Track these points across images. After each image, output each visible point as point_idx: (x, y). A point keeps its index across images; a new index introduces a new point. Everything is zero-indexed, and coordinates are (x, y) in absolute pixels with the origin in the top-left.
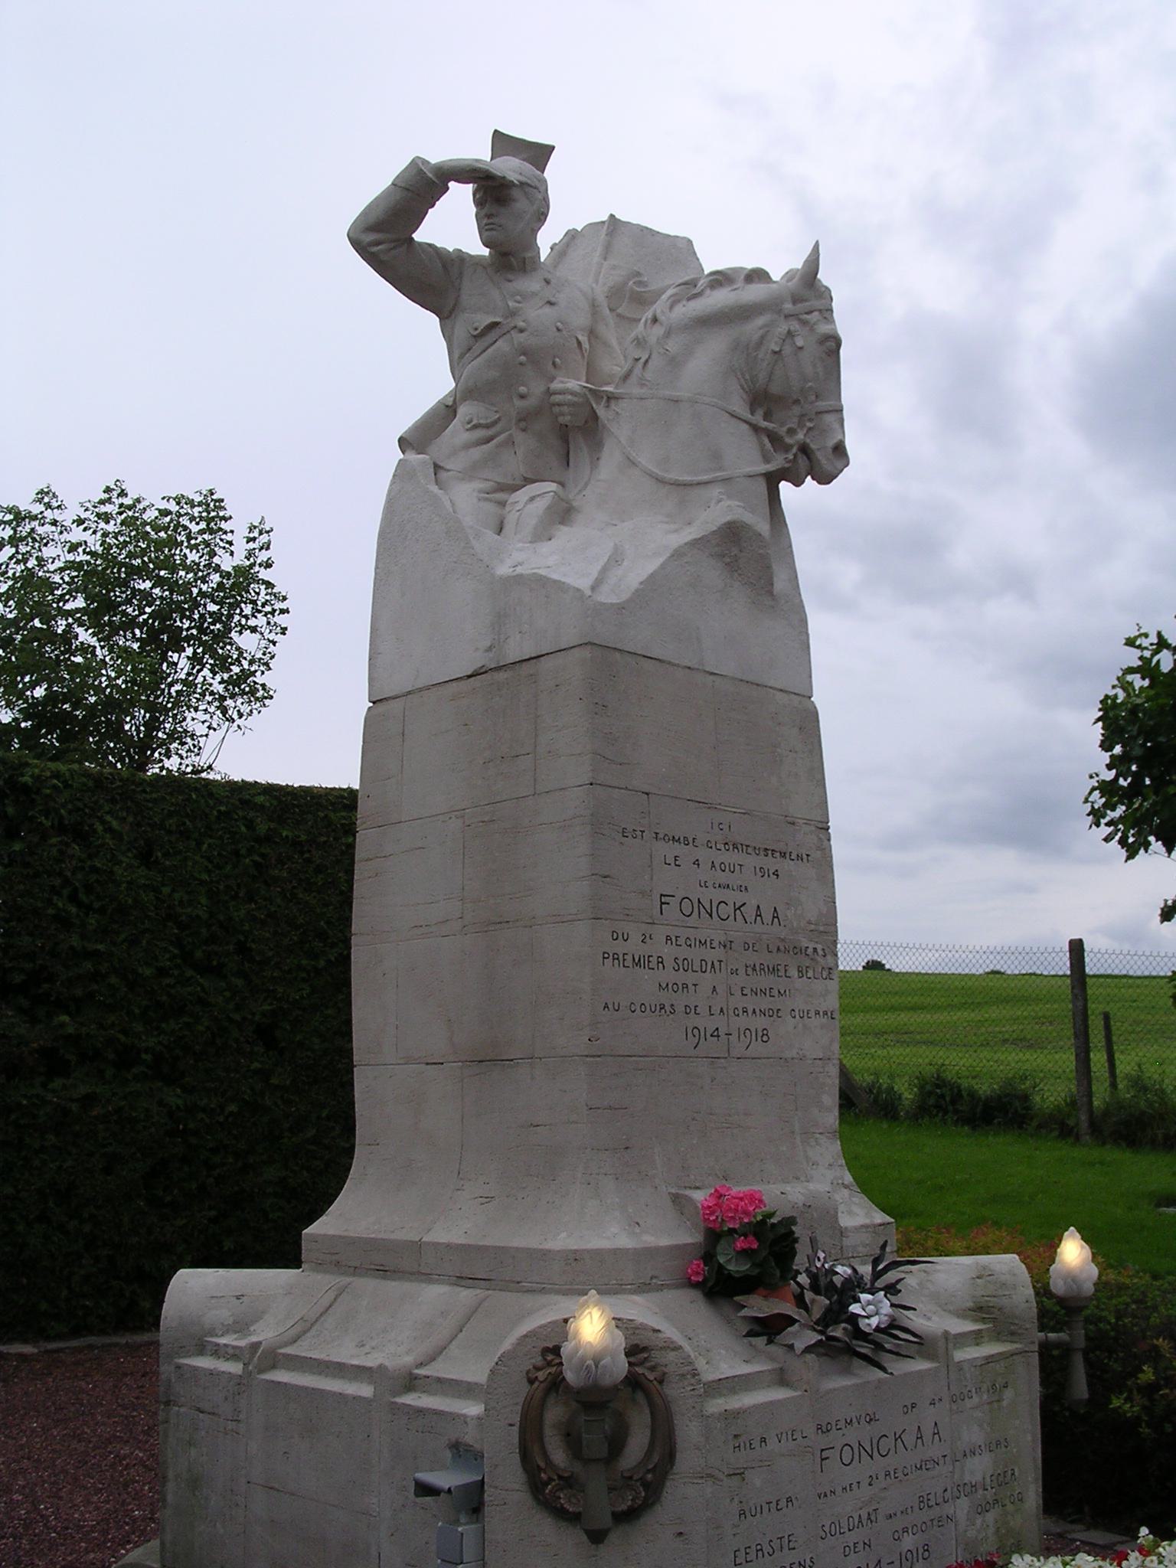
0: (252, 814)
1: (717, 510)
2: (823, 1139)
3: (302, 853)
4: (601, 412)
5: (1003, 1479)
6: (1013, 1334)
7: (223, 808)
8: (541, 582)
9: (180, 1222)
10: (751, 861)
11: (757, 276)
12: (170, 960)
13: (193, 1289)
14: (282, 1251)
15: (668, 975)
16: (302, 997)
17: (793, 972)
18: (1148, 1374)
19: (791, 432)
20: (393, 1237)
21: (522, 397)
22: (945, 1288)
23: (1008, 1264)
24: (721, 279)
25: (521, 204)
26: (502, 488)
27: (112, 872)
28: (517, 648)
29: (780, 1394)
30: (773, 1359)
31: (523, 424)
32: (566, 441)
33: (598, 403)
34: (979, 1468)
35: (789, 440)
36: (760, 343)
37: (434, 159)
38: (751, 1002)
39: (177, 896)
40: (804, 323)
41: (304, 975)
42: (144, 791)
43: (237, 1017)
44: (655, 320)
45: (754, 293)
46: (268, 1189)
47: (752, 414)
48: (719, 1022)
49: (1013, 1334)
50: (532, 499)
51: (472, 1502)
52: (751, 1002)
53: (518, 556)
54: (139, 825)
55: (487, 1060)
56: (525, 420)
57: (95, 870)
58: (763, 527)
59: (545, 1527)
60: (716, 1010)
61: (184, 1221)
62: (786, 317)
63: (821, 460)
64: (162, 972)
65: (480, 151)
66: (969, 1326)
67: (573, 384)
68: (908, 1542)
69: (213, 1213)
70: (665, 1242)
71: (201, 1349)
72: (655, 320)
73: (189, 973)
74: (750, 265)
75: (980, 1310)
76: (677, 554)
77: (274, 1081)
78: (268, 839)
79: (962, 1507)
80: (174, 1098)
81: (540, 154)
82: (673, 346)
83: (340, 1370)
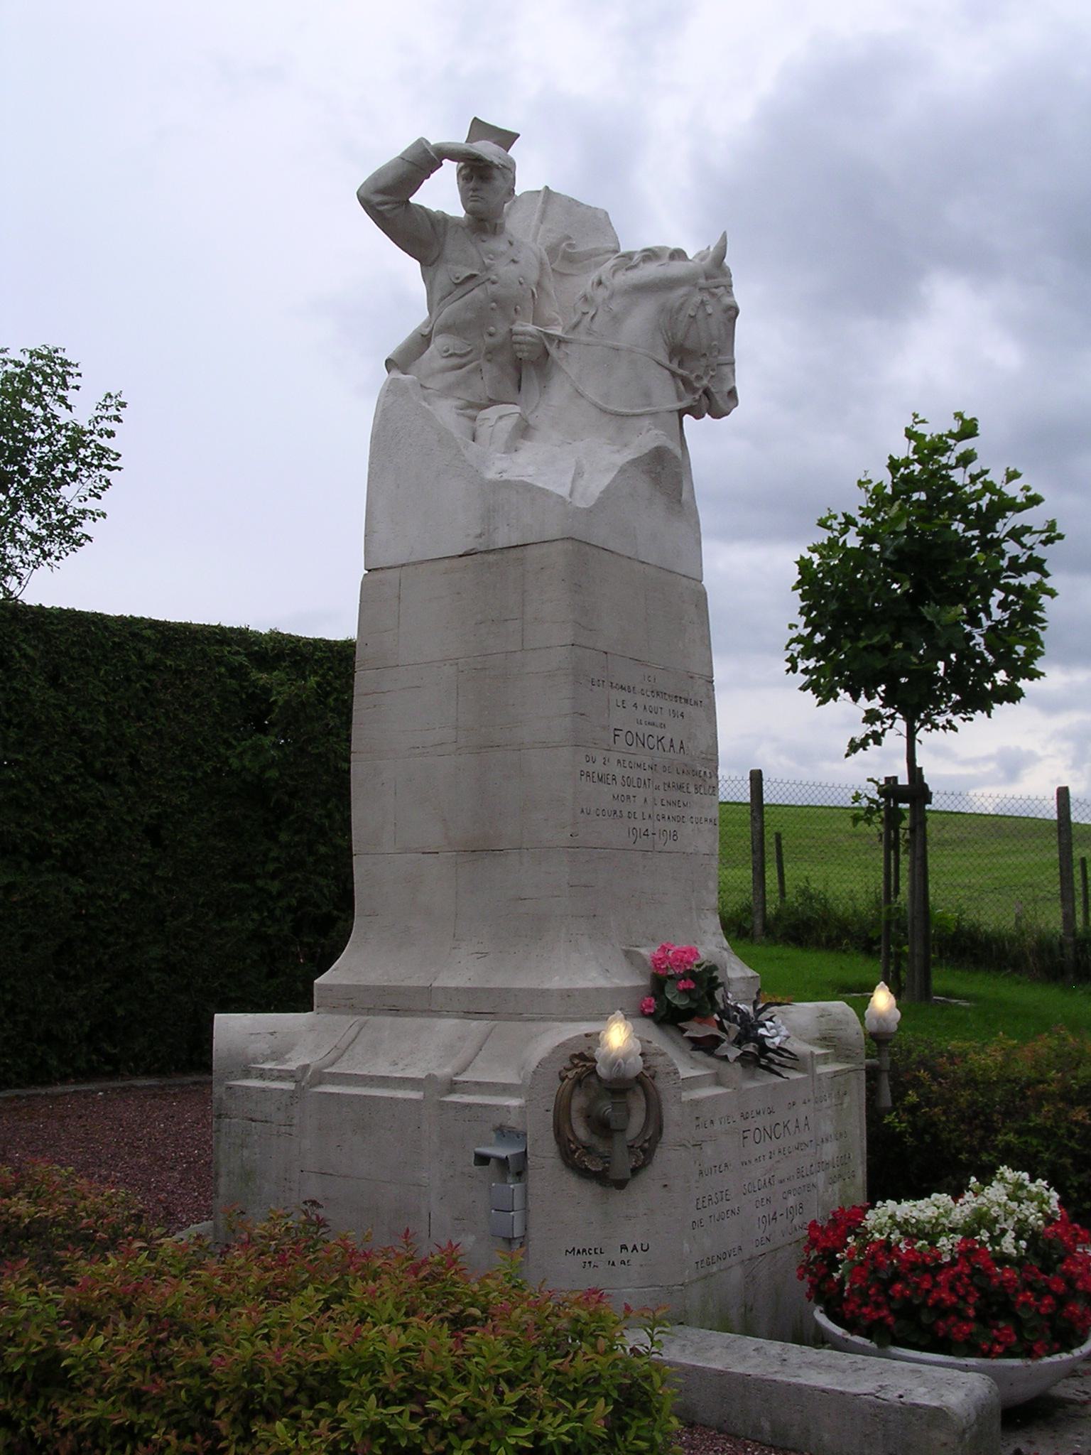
0: (141, 645)
1: (648, 438)
2: (709, 914)
3: (182, 680)
4: (553, 350)
5: (844, 1160)
6: (848, 1057)
7: (116, 640)
8: (527, 488)
9: (81, 993)
10: (667, 704)
11: (678, 254)
12: (75, 769)
13: (233, 1029)
14: (300, 1000)
15: (618, 789)
16: (182, 802)
17: (692, 789)
18: (912, 1097)
19: (699, 378)
20: (403, 984)
21: (491, 335)
22: (793, 1023)
23: (838, 1007)
24: (651, 255)
25: (499, 182)
26: (470, 405)
27: (28, 693)
28: (501, 540)
29: (719, 1091)
30: (709, 1067)
31: (489, 356)
32: (519, 370)
33: (551, 344)
34: (830, 1151)
35: (697, 385)
36: (680, 309)
37: (433, 141)
38: (667, 811)
39: (80, 714)
40: (713, 295)
41: (184, 784)
42: (52, 623)
43: (129, 819)
44: (600, 283)
45: (677, 269)
46: (291, 948)
47: (671, 361)
48: (648, 824)
49: (848, 1057)
50: (501, 417)
51: (516, 1168)
52: (667, 811)
53: (499, 465)
54: (48, 652)
55: (480, 849)
56: (491, 353)
57: (15, 690)
58: (678, 452)
59: (571, 1183)
60: (646, 816)
61: (85, 992)
62: (701, 289)
63: (713, 399)
64: (69, 779)
65: (457, 136)
66: (819, 1051)
67: (531, 328)
68: (792, 1200)
69: (108, 985)
70: (627, 984)
71: (247, 1074)
72: (600, 283)
73: (90, 781)
74: (673, 246)
75: (825, 1040)
76: (622, 470)
77: (159, 873)
78: (153, 667)
79: (820, 1178)
80: (78, 886)
81: (507, 139)
82: (616, 306)
83: (384, 1081)
